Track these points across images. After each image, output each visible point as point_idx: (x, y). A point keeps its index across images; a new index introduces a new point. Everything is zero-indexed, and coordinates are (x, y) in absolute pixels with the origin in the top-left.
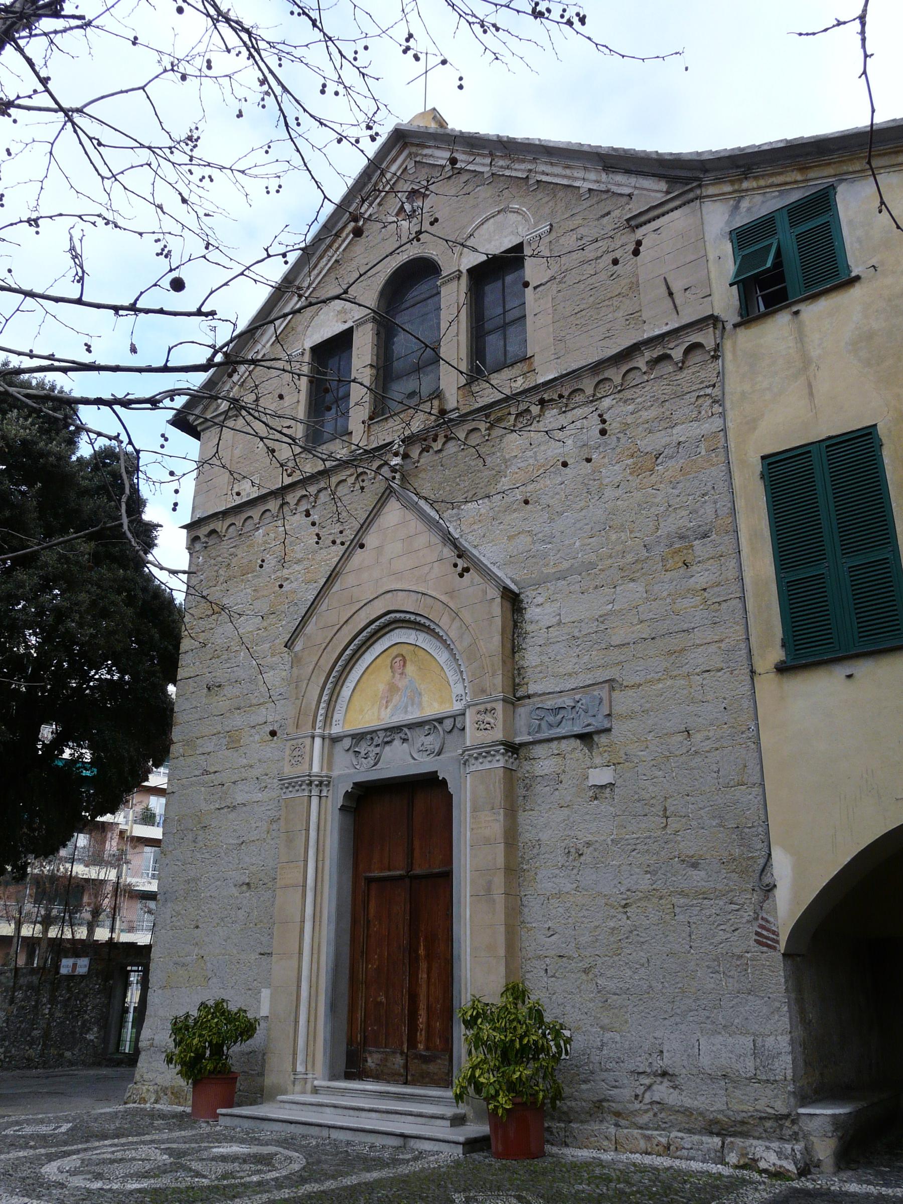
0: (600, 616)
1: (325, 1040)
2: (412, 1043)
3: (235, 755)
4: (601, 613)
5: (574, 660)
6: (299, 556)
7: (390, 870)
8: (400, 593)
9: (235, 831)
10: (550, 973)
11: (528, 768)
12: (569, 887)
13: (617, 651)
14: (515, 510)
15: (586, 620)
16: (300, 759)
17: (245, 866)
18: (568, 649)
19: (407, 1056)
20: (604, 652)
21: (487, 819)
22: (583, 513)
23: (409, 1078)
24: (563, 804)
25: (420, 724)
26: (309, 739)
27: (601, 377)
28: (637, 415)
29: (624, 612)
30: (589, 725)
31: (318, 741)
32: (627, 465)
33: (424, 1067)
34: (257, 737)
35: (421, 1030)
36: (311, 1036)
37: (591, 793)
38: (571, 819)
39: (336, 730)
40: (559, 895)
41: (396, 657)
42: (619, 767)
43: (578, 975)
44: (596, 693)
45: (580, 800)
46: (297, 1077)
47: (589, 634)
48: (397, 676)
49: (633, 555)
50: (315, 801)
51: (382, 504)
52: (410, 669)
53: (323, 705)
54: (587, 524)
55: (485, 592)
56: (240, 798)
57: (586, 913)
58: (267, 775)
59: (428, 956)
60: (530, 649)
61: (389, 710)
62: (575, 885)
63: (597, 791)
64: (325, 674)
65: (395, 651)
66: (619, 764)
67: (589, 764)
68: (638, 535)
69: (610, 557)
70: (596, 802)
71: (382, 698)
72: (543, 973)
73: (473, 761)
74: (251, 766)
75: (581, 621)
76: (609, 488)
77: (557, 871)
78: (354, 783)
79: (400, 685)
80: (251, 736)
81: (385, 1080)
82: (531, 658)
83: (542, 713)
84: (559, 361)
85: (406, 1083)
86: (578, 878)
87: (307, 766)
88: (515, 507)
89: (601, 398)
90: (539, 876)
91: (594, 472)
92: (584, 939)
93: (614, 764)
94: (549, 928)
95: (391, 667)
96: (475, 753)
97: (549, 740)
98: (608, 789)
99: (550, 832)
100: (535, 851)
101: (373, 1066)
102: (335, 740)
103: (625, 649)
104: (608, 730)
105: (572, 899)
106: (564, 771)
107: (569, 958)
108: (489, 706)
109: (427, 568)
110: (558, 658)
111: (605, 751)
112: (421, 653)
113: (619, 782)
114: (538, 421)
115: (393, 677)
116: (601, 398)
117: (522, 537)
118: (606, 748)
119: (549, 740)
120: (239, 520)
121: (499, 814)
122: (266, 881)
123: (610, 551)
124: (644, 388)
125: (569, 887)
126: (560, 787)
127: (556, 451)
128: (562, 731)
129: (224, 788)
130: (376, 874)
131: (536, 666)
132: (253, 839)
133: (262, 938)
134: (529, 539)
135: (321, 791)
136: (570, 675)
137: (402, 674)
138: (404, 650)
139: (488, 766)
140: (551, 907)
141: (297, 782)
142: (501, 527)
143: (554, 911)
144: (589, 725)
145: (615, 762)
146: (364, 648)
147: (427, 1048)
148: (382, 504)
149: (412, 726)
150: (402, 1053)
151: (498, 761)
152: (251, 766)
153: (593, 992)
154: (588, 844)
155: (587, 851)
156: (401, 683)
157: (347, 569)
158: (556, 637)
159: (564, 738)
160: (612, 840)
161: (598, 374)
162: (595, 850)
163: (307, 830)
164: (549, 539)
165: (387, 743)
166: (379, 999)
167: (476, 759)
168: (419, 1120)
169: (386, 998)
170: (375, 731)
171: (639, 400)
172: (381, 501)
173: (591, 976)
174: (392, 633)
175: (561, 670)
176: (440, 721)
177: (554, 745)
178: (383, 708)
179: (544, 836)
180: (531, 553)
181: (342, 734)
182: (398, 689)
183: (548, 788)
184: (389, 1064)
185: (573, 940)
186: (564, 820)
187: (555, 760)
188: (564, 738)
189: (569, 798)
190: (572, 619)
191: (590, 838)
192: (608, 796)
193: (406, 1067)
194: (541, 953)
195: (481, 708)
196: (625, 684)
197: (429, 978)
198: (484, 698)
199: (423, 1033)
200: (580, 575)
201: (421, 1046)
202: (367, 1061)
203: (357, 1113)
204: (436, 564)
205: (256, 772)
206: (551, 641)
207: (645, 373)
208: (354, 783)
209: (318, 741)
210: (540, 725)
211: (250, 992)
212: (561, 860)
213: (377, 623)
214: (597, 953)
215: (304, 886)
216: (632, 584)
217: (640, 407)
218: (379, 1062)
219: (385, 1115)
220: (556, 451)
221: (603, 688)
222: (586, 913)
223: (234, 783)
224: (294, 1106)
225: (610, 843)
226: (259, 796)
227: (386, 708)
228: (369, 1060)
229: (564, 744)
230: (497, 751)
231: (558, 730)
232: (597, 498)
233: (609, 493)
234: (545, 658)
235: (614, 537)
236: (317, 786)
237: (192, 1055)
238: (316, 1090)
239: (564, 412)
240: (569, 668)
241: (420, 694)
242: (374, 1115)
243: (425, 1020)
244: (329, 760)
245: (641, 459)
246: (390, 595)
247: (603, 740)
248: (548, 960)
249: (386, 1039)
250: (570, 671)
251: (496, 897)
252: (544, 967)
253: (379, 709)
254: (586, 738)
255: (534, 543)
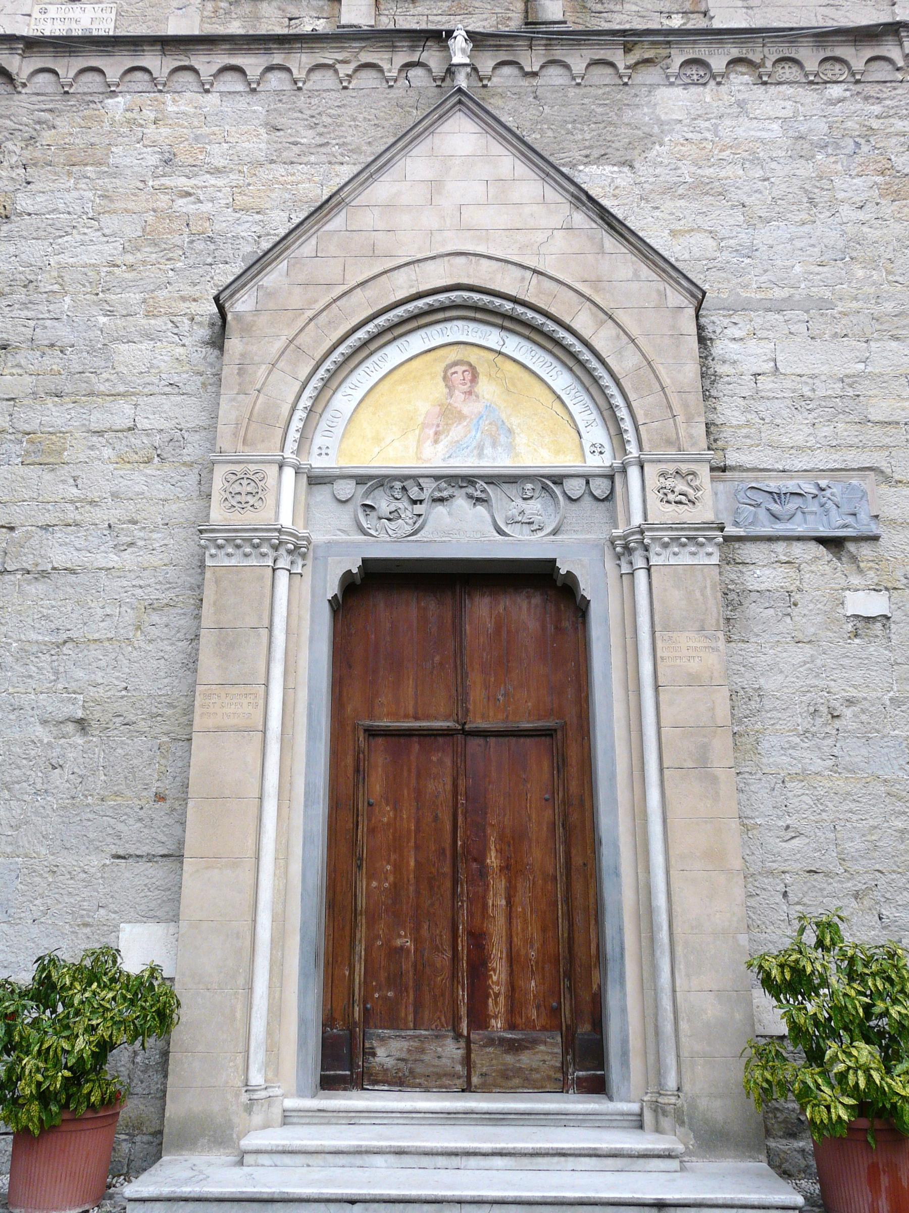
0: (847, 376)
1: (302, 1021)
2: (479, 1019)
3: (47, 476)
4: (848, 371)
5: (807, 430)
6: (220, 162)
7: (416, 718)
8: (484, 261)
9: (46, 617)
10: (792, 897)
11: (733, 577)
12: (818, 765)
13: (878, 430)
14: (681, 197)
15: (823, 378)
16: (252, 500)
17: (73, 686)
18: (795, 412)
19: (468, 1041)
20: (858, 427)
21: (691, 644)
22: (807, 228)
23: (475, 1080)
24: (800, 637)
25: (513, 479)
26: (276, 467)
27: (829, 54)
28: (886, 121)
29: (886, 378)
30: (846, 526)
31: (289, 473)
32: (876, 183)
33: (509, 1059)
34: (107, 452)
35: (497, 995)
36: (275, 1012)
37: (849, 627)
38: (819, 662)
39: (318, 463)
40: (802, 776)
41: (455, 364)
42: (895, 594)
43: (846, 901)
44: (854, 482)
45: (829, 634)
46: (255, 1096)
47: (830, 397)
48: (459, 396)
49: (893, 304)
50: (283, 578)
51: (440, 117)
52: (486, 388)
53: (300, 414)
54: (813, 246)
55: (663, 295)
56: (60, 557)
57: (853, 806)
58: (135, 523)
59: (506, 868)
60: (725, 399)
61: (441, 446)
62: (829, 763)
63: (859, 625)
64: (313, 363)
65: (453, 354)
66: (895, 589)
67: (844, 583)
68: (900, 279)
69: (856, 298)
70: (857, 641)
71: (424, 426)
72: (779, 898)
73: (658, 549)
74: (92, 503)
75: (813, 377)
76: (846, 206)
77: (798, 740)
78: (364, 560)
79: (465, 410)
80: (92, 448)
81: (419, 1085)
82: (728, 412)
83: (759, 497)
84: (750, 11)
85: (468, 1089)
86: (835, 751)
87: (272, 515)
88: (680, 191)
89: (826, 82)
90: (765, 745)
91: (821, 178)
92: (853, 846)
93: (887, 589)
94: (788, 827)
95: (445, 378)
96: (666, 536)
97: (770, 539)
98: (879, 625)
99: (780, 678)
100: (753, 705)
101: (390, 1063)
102: (316, 480)
103: (891, 430)
104: (875, 538)
105: (825, 782)
106: (799, 590)
107: (827, 875)
108: (684, 468)
109: (540, 236)
110: (778, 421)
111: (870, 568)
112: (510, 366)
113: (897, 616)
114: (719, 84)
115: (451, 395)
116: (826, 82)
117: (698, 237)
118: (871, 564)
119: (770, 539)
120: (68, 67)
121: (717, 639)
122: (131, 717)
123: (856, 292)
124: (895, 89)
125: (818, 765)
126: (795, 611)
127: (752, 133)
128: (798, 527)
129: (15, 534)
130: (385, 723)
131: (739, 427)
132: (96, 636)
133: (121, 827)
134: (711, 243)
135: (292, 563)
136: (799, 448)
137: (470, 393)
138: (473, 356)
139: (689, 560)
140: (790, 794)
141: (250, 540)
142: (657, 213)
143: (795, 801)
144: (846, 526)
145: (889, 585)
146: (389, 336)
147: (512, 1027)
148: (440, 117)
149: (493, 480)
150: (458, 1036)
151: (709, 554)
152: (92, 503)
153: (874, 928)
154: (850, 702)
155: (848, 712)
156: (469, 408)
157: (362, 199)
158: (770, 390)
159: (799, 539)
160: (891, 699)
161: (824, 48)
162: (863, 711)
163: (270, 628)
164: (751, 252)
165: (441, 500)
166: (399, 942)
167: (666, 546)
168: (610, 1163)
169: (417, 940)
170: (414, 477)
171: (888, 102)
172: (440, 111)
173: (867, 902)
174: (448, 325)
175: (784, 439)
176: (558, 480)
177: (780, 547)
178: (429, 443)
179: (769, 684)
180: (715, 263)
181: (337, 472)
182: (461, 417)
183: (771, 611)
184: (426, 1058)
185: (832, 847)
186: (805, 663)
187: (782, 570)
188: (799, 539)
189: (812, 630)
190: (799, 371)
191: (853, 693)
192: (879, 633)
193: (467, 1061)
194: (775, 865)
195: (671, 468)
196: (897, 477)
197: (509, 903)
198: (672, 452)
199: (502, 999)
200: (807, 312)
201: (497, 1024)
202: (374, 1055)
203: (455, 1161)
204: (559, 234)
205: (101, 515)
206: (763, 394)
207: (898, 69)
208: (364, 560)
209: (289, 473)
210: (755, 514)
211: (87, 930)
212: (805, 723)
213: (430, 300)
214: (877, 867)
215: (657, 687)
216: (894, 344)
217: (892, 112)
218: (404, 1055)
219: (526, 1161)
220: (752, 133)
221: (866, 477)
222: (853, 806)
223: (46, 527)
224: (287, 1159)
225: (888, 702)
226: (113, 560)
227: (436, 442)
228: (381, 1052)
229: (797, 549)
230: (710, 539)
231: (789, 526)
232: (828, 214)
233: (846, 212)
234: (752, 417)
235: (860, 273)
236: (290, 552)
237: (67, 1073)
238: (287, 1118)
239: (765, 83)
240: (799, 439)
241: (510, 431)
242: (498, 1162)
243: (504, 977)
244: (304, 511)
245: (897, 181)
246: (462, 260)
247: (865, 551)
248: (788, 878)
249: (416, 1013)
250: (801, 443)
251: (718, 772)
252: (781, 888)
253: (419, 443)
254: (833, 544)
255: (721, 249)
